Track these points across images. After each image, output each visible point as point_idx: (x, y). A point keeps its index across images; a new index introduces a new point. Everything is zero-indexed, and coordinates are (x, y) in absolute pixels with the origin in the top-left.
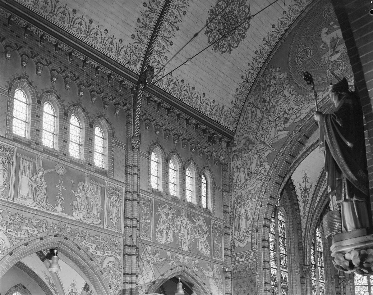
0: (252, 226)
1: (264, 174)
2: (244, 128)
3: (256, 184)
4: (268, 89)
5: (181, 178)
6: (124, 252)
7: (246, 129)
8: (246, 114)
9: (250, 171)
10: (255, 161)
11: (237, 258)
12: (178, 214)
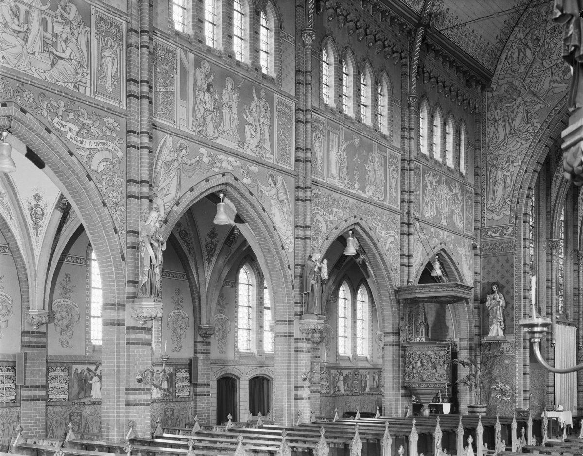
0: (511, 195)
1: (532, 134)
2: (507, 69)
3: (519, 144)
4: (543, 25)
5: (252, 29)
6: (401, 230)
7: (510, 71)
8: (510, 52)
9: (513, 126)
10: (520, 116)
11: (489, 233)
12: (439, 181)
